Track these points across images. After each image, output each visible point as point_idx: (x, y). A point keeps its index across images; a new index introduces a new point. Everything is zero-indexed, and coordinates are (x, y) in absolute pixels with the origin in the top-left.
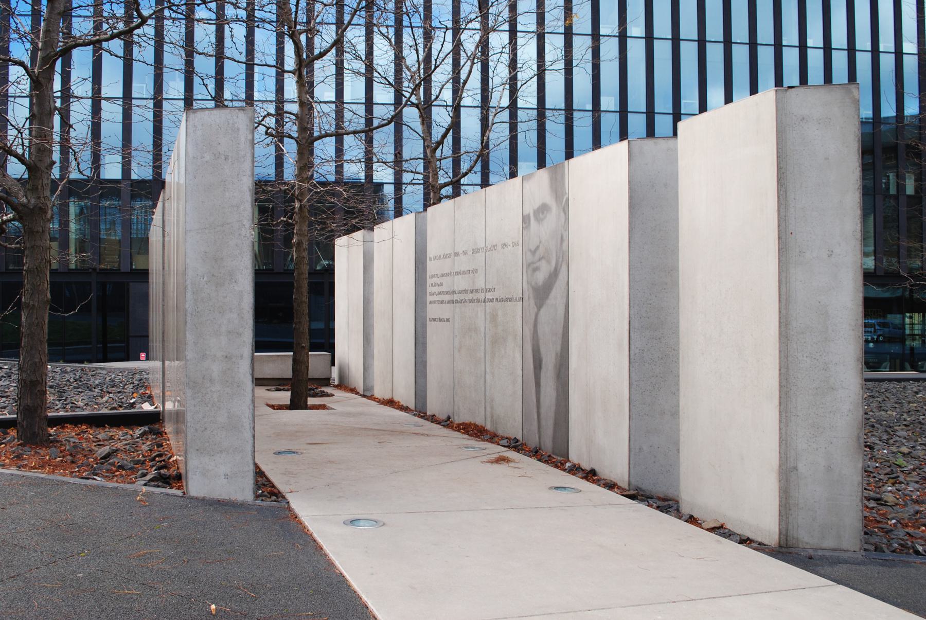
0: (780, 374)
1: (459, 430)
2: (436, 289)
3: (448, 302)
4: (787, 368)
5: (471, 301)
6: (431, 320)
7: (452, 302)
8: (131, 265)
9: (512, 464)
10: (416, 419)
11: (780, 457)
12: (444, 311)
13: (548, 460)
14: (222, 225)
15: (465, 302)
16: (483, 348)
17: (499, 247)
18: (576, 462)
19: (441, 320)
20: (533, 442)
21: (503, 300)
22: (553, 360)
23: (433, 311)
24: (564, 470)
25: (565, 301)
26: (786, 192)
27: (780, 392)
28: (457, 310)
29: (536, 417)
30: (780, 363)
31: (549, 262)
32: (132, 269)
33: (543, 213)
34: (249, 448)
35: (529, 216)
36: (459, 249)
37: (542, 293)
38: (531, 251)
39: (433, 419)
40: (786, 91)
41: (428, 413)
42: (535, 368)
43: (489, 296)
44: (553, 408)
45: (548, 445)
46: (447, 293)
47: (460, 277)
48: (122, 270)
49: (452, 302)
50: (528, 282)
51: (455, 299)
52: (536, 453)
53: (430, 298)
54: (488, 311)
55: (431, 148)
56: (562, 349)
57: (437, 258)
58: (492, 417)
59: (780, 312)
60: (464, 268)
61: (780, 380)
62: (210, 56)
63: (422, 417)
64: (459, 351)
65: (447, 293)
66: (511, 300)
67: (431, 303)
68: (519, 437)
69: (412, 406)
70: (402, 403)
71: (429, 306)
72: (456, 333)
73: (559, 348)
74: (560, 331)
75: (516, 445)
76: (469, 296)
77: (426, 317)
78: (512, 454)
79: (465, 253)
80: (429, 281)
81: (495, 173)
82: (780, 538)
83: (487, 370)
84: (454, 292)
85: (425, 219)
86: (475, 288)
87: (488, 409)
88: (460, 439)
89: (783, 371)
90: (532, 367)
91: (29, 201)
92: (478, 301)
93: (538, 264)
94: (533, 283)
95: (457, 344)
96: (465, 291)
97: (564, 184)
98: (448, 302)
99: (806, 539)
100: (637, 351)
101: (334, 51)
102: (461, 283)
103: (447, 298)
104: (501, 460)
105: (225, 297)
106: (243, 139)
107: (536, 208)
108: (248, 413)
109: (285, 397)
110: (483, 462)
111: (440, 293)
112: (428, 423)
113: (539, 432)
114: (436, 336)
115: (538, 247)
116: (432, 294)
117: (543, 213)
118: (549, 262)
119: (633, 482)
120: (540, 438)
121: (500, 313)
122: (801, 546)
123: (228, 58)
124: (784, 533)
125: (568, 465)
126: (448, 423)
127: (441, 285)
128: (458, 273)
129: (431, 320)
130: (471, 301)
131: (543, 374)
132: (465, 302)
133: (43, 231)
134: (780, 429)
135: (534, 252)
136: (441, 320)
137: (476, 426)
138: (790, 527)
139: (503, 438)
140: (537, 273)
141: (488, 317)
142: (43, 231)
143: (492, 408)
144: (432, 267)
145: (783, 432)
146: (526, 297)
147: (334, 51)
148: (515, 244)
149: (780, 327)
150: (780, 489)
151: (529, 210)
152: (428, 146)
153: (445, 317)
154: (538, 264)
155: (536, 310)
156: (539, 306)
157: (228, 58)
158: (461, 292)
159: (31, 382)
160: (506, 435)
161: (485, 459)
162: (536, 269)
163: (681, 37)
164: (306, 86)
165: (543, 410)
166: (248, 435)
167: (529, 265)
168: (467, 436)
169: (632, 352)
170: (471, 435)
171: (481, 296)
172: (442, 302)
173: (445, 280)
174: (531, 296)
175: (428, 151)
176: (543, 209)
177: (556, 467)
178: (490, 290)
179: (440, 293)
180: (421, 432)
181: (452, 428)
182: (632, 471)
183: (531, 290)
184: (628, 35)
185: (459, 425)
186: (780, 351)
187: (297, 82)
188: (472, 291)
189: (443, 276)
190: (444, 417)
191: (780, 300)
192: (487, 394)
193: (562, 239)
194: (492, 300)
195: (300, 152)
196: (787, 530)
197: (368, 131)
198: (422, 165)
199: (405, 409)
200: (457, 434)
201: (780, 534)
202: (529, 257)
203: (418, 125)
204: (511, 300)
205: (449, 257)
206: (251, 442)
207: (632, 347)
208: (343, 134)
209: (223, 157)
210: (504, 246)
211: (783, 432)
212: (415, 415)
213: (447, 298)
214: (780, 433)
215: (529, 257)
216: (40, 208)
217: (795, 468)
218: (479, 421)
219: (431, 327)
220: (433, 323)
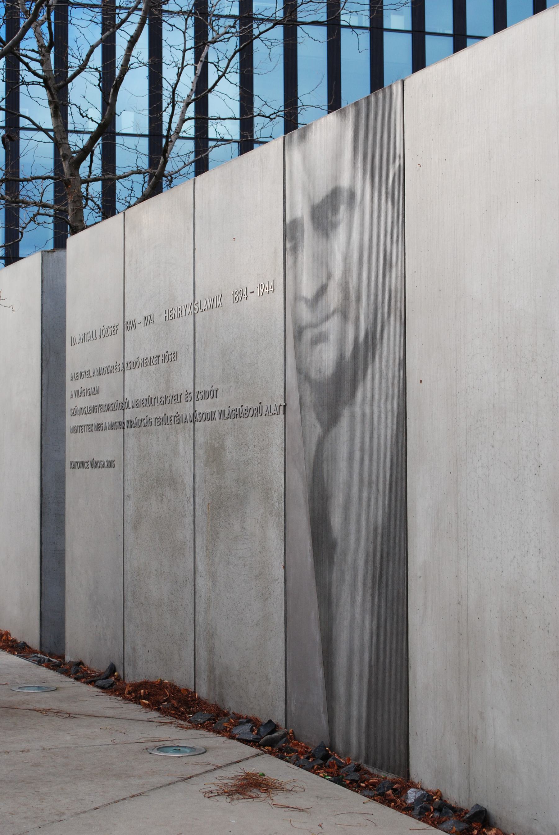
1: (137, 700)
2: (84, 402)
3: (112, 427)
5: (163, 421)
6: (75, 465)
7: (120, 425)
9: (279, 798)
10: (44, 672)
12: (105, 446)
13: (354, 779)
15: (149, 423)
16: (189, 519)
17: (229, 299)
18: (430, 785)
19: (95, 465)
20: (314, 731)
21: (236, 414)
22: (366, 543)
23: (76, 447)
24: (407, 810)
25: (395, 404)
28: (131, 442)
29: (320, 674)
31: (352, 320)
33: (335, 210)
35: (299, 223)
36: (135, 313)
37: (333, 393)
38: (304, 299)
39: (78, 672)
41: (68, 658)
42: (317, 561)
43: (203, 407)
44: (366, 657)
45: (352, 739)
46: (109, 408)
47: (137, 371)
49: (120, 425)
50: (298, 370)
51: (126, 419)
52: (323, 760)
53: (71, 421)
54: (201, 439)
55: (67, 163)
56: (389, 516)
57: (87, 337)
58: (212, 669)
60: (148, 350)
63: (55, 667)
64: (135, 528)
65: (109, 408)
66: (257, 412)
67: (74, 430)
68: (279, 718)
69: (33, 641)
70: (13, 636)
71: (70, 438)
72: (129, 491)
73: (380, 517)
74: (385, 475)
75: (271, 739)
76: (158, 412)
77: (64, 460)
78: (270, 766)
79: (149, 320)
80: (71, 386)
83: (200, 567)
84: (123, 406)
85: (62, 263)
86: (173, 391)
87: (202, 653)
88: (146, 727)
90: (310, 560)
92: (179, 419)
93: (323, 327)
94: (311, 372)
95: (129, 513)
96: (149, 401)
97: (390, 135)
98: (112, 427)
102: (139, 385)
103: (109, 418)
104: (252, 786)
107: (317, 200)
110: (209, 795)
111: (93, 410)
112: (67, 683)
113: (330, 710)
114: (87, 502)
115: (323, 289)
116: (76, 413)
117: (335, 210)
118: (352, 320)
120: (330, 722)
121: (229, 442)
125: (412, 795)
126: (109, 681)
127: (96, 391)
128: (133, 365)
129: (75, 465)
130: (163, 421)
131: (337, 576)
132: (149, 423)
135: (312, 303)
136: (95, 465)
137: (175, 689)
139: (239, 720)
140: (322, 347)
141: (200, 452)
143: (211, 651)
144: (75, 357)
146: (294, 403)
148: (265, 289)
151: (300, 208)
152: (65, 156)
153: (105, 457)
154: (323, 327)
155: (318, 430)
156: (327, 422)
158: (138, 404)
160: (245, 713)
161: (211, 782)
162: (316, 340)
163: (469, 33)
165: (339, 659)
167: (300, 332)
168: (155, 714)
170: (164, 712)
171: (186, 409)
172: (99, 427)
173: (103, 382)
174: (307, 400)
175: (65, 166)
176: (338, 201)
177: (385, 800)
178: (206, 395)
179: (93, 410)
180: (54, 706)
181: (121, 694)
183: (305, 386)
184: (385, 26)
185: (137, 687)
188: (165, 400)
189: (100, 372)
190: (103, 667)
192: (200, 619)
193: (388, 256)
194: (210, 417)
198: (51, 188)
199: (19, 648)
200: (133, 710)
202: (301, 311)
203: (45, 117)
204: (257, 412)
205: (114, 333)
210: (240, 295)
212: (40, 663)
213: (109, 418)
215: (301, 311)
218: (181, 677)
219: (75, 482)
220: (79, 472)
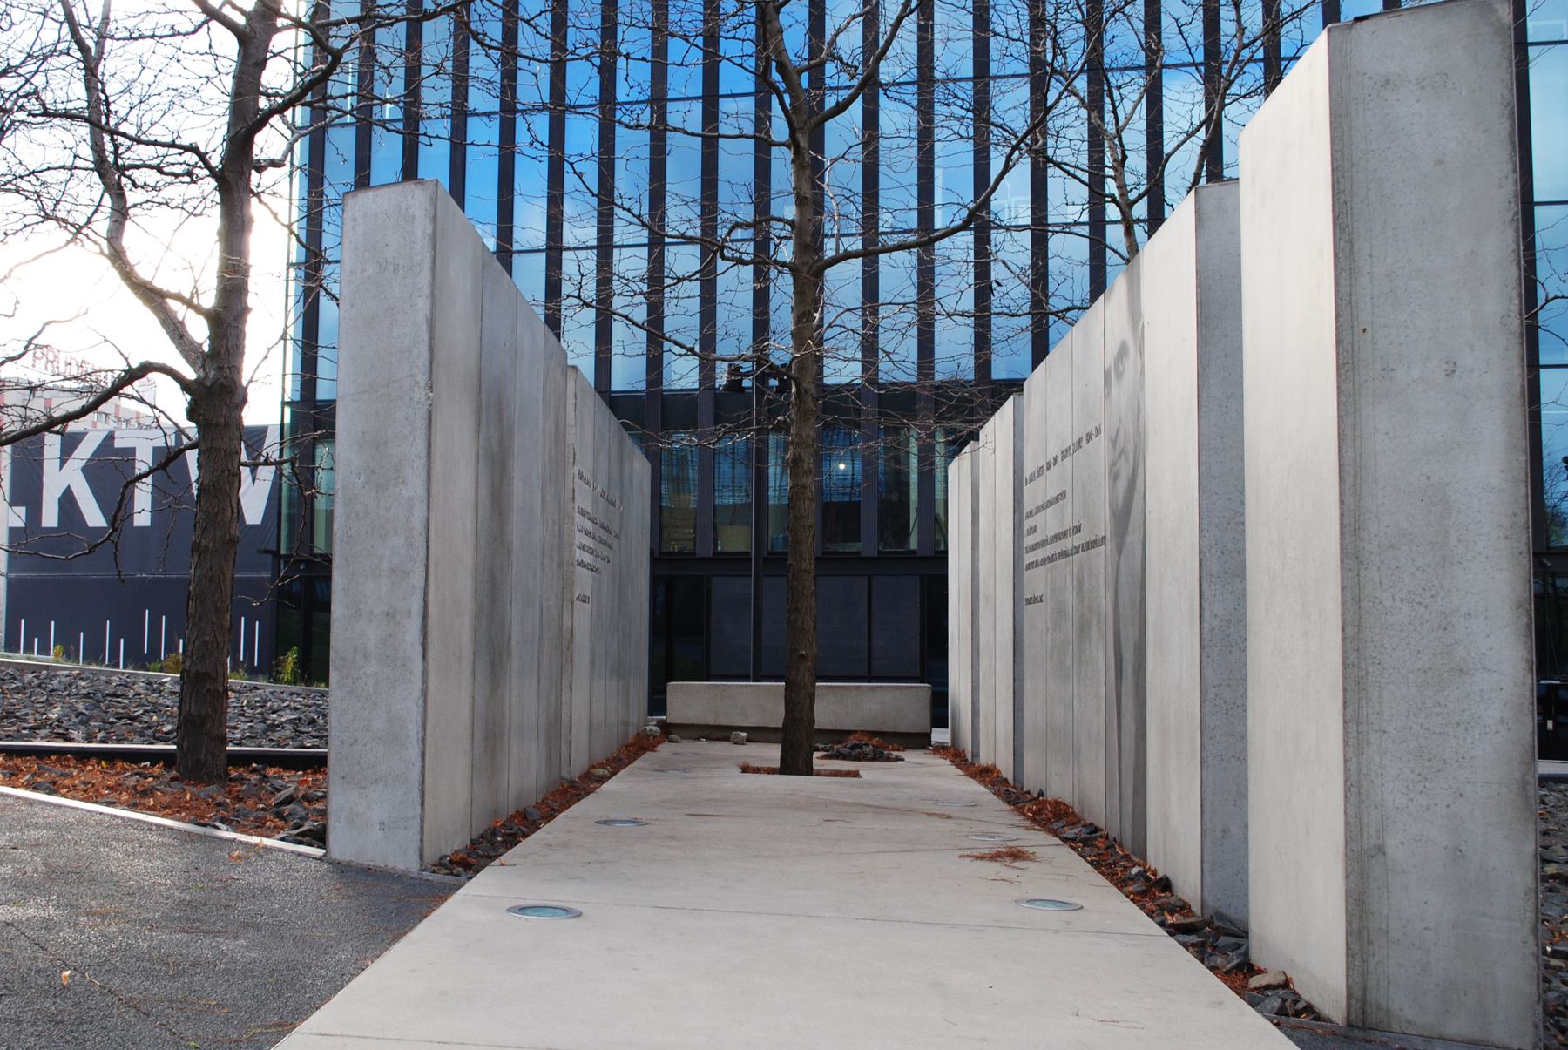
0: (1344, 639)
4: (1359, 626)
8: (715, 545)
11: (1347, 824)
14: (388, 386)
26: (1351, 242)
27: (1344, 678)
30: (1343, 615)
32: (716, 553)
34: (415, 775)
40: (1350, 26)
48: (699, 554)
59: (1342, 502)
61: (1344, 651)
62: (693, 134)
68: (1101, 824)
81: (573, 220)
82: (1349, 1005)
89: (1350, 631)
91: (207, 375)
99: (1408, 1013)
100: (1216, 623)
101: (859, 101)
105: (388, 509)
106: (419, 234)
108: (415, 713)
109: (771, 753)
119: (1210, 902)
122: (1396, 1028)
123: (675, 129)
124: (1358, 994)
133: (226, 424)
134: (1346, 761)
138: (1371, 983)
142: (226, 424)
145: (1353, 767)
147: (859, 101)
149: (1342, 533)
150: (1349, 895)
157: (675, 129)
159: (197, 674)
164: (810, 168)
166: (414, 752)
169: (1206, 625)
182: (1207, 879)
186: (1343, 589)
187: (793, 161)
191: (1341, 478)
195: (799, 292)
196: (1364, 989)
197: (926, 238)
201: (1349, 996)
206: (418, 765)
207: (1207, 614)
208: (877, 253)
209: (391, 268)
211: (1353, 767)
214: (1347, 770)
216: (222, 385)
217: (1381, 850)
